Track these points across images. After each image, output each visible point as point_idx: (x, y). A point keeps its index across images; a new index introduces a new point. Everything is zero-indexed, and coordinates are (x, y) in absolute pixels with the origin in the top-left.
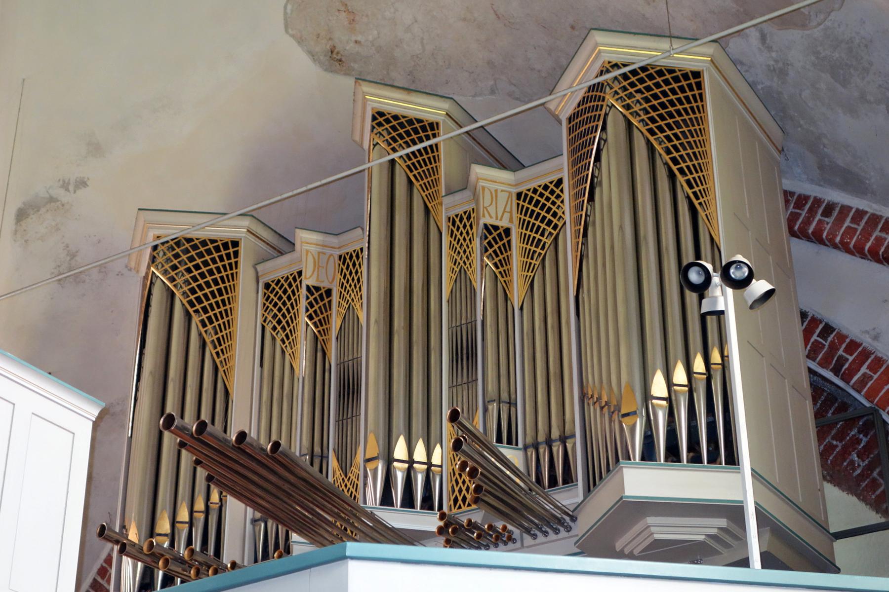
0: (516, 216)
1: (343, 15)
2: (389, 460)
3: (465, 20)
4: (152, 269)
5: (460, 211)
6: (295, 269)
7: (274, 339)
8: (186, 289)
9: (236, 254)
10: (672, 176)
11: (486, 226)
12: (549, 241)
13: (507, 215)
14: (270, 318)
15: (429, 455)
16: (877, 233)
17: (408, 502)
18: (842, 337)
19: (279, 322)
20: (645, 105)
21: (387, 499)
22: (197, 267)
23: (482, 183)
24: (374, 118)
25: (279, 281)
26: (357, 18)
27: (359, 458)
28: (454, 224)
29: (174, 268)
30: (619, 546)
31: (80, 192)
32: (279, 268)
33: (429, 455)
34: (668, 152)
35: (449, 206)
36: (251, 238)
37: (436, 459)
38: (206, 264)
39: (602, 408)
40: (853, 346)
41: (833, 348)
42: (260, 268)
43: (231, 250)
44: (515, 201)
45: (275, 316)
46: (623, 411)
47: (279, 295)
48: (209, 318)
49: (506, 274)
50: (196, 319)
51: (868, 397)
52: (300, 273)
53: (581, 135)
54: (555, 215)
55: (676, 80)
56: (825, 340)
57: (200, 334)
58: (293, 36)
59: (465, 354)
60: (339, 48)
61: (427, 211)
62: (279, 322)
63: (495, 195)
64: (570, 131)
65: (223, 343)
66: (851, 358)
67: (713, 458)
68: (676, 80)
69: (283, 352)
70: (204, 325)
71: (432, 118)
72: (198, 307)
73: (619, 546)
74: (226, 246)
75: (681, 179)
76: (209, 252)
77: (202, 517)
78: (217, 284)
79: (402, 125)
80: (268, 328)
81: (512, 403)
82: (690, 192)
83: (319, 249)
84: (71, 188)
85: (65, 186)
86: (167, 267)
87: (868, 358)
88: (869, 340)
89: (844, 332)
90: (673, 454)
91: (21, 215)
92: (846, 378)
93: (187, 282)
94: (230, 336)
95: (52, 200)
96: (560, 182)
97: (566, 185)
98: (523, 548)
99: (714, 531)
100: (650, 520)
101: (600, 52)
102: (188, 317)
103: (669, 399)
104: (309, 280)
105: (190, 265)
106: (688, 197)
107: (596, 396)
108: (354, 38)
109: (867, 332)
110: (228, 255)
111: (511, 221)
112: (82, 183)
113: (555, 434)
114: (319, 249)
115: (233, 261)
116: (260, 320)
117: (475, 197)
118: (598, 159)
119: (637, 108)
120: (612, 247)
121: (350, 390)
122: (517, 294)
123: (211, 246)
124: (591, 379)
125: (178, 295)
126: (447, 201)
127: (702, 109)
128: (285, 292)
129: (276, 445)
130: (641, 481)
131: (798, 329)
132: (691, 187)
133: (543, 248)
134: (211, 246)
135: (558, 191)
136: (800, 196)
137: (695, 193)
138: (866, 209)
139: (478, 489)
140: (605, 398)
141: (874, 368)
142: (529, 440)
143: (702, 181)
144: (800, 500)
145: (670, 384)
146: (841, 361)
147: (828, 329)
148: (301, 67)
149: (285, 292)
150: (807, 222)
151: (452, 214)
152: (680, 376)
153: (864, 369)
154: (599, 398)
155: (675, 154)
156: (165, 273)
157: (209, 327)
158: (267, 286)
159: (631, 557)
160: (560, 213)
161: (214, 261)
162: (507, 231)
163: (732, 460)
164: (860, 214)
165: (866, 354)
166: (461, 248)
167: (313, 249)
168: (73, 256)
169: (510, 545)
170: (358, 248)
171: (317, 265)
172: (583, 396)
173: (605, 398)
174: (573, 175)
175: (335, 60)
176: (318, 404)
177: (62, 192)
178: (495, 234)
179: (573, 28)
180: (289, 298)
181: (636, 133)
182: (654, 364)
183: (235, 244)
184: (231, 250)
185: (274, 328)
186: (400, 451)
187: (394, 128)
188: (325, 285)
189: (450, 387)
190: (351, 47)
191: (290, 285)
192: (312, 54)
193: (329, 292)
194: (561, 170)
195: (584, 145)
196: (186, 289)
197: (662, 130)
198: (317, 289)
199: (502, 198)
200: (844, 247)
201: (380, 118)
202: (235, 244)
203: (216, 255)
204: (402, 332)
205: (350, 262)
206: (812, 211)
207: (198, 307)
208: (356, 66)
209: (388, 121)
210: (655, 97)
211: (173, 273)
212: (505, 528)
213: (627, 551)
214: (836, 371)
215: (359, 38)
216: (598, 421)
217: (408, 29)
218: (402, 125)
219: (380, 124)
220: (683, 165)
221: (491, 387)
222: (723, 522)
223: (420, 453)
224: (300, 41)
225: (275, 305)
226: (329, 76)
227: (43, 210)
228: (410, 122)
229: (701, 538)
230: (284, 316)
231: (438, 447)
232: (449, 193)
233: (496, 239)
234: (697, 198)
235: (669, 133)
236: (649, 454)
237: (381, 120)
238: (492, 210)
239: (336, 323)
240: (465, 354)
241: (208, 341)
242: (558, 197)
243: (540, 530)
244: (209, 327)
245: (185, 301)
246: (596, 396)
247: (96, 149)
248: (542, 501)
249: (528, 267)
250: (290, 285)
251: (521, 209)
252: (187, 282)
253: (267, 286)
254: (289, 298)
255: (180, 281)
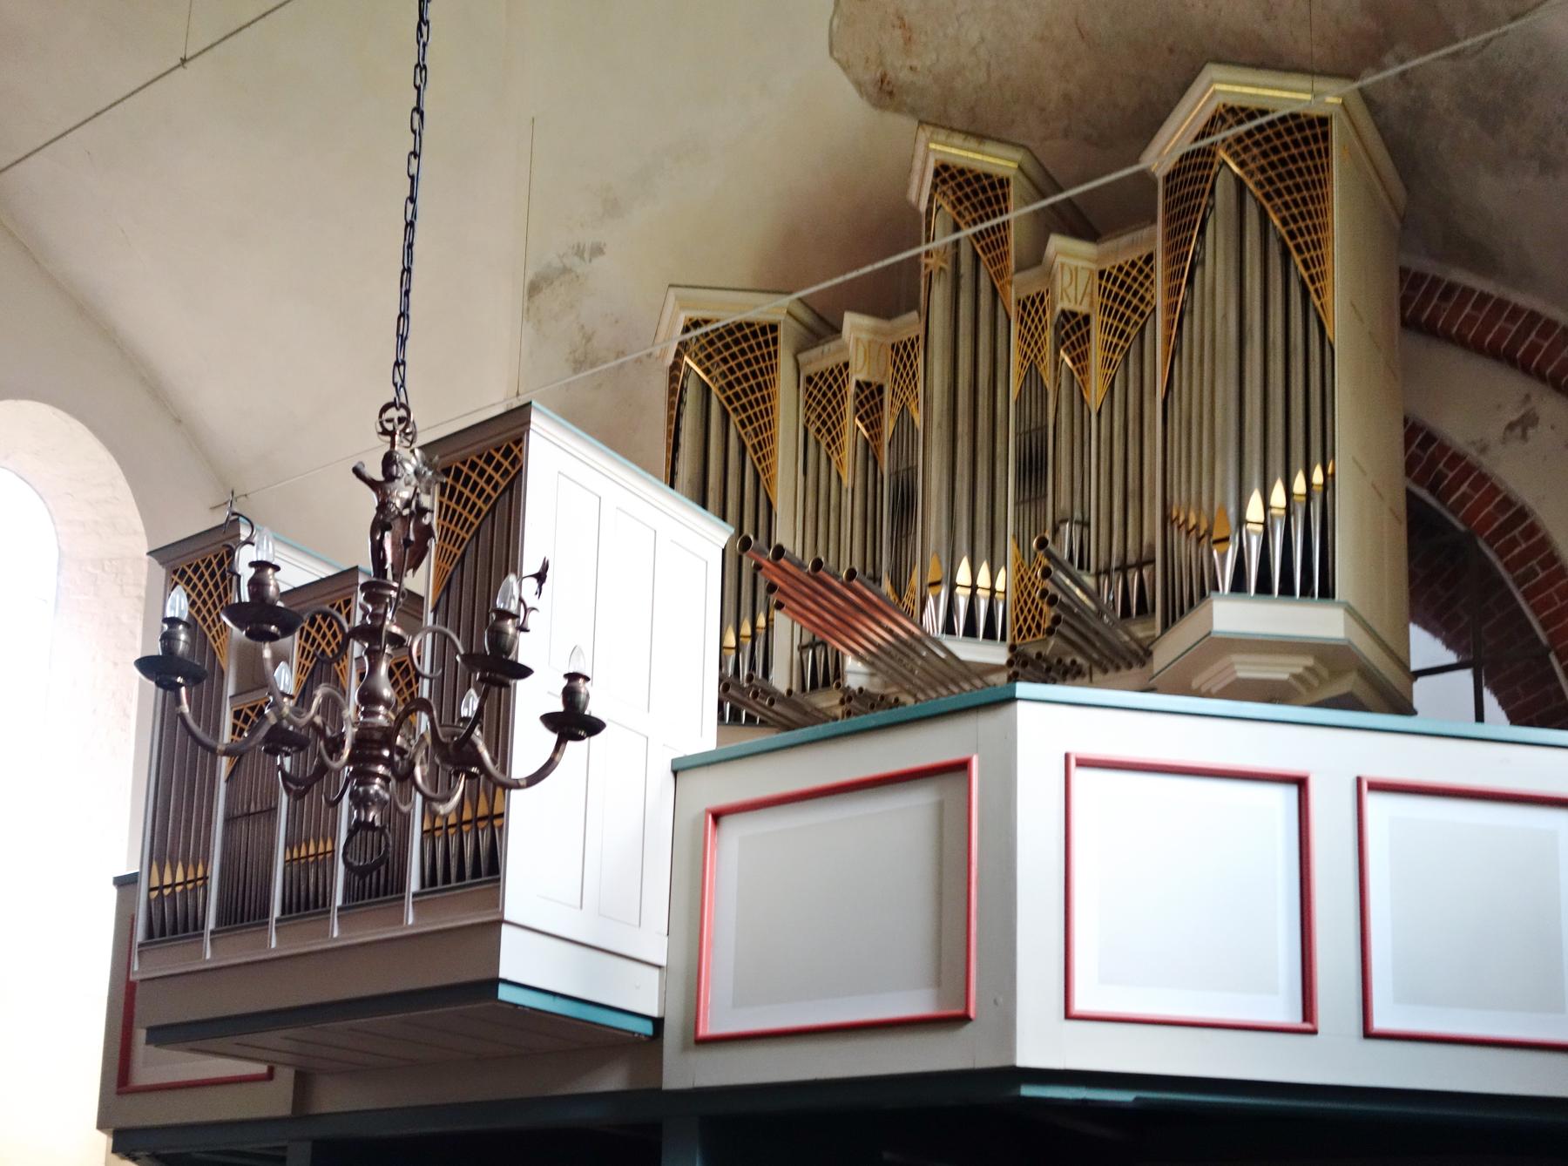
0: (1098, 299)
1: (898, 32)
2: (953, 586)
3: (1042, 39)
4: (686, 359)
5: (1033, 293)
6: (841, 360)
7: (818, 443)
8: (723, 382)
9: (775, 341)
10: (1286, 254)
11: (1063, 312)
12: (1134, 332)
13: (1086, 301)
14: (813, 418)
15: (993, 579)
16: (1500, 323)
17: (970, 631)
18: (1444, 448)
19: (824, 423)
20: (1263, 162)
21: (949, 629)
22: (734, 357)
23: (1059, 259)
24: (937, 173)
25: (822, 374)
26: (915, 36)
27: (916, 580)
28: (1024, 307)
29: (709, 357)
30: (1195, 685)
31: (597, 261)
32: (821, 359)
33: (993, 579)
34: (1284, 222)
35: (1017, 287)
36: (791, 321)
37: (1000, 586)
38: (743, 352)
39: (1188, 533)
40: (1456, 458)
41: (1433, 461)
42: (802, 357)
43: (770, 336)
44: (1097, 281)
45: (819, 416)
46: (1216, 536)
47: (823, 391)
48: (749, 418)
49: (1083, 371)
50: (734, 418)
51: (1463, 521)
52: (846, 365)
53: (1181, 200)
54: (1142, 299)
55: (1300, 128)
56: (1425, 450)
57: (739, 437)
58: (838, 61)
59: (1033, 468)
60: (891, 75)
61: (994, 292)
62: (824, 423)
63: (1075, 272)
64: (1167, 194)
65: (764, 447)
66: (1451, 475)
67: (1307, 591)
68: (1300, 128)
69: (829, 459)
70: (744, 426)
71: (1001, 173)
72: (737, 404)
73: (1195, 685)
74: (763, 330)
75: (1297, 259)
76: (746, 338)
77: (749, 642)
78: (755, 376)
79: (969, 183)
80: (812, 430)
81: (1085, 524)
82: (1306, 275)
83: (870, 337)
84: (586, 256)
85: (579, 252)
86: (701, 356)
87: (1470, 474)
88: (1474, 453)
89: (1448, 443)
90: (1264, 587)
91: (534, 289)
92: (1442, 499)
93: (724, 375)
94: (772, 439)
95: (565, 270)
96: (1149, 259)
97: (1159, 262)
98: (1092, 683)
99: (1299, 670)
100: (1235, 658)
101: (1215, 92)
102: (725, 416)
103: (1265, 524)
104: (858, 374)
105: (726, 354)
106: (1302, 282)
107: (1182, 519)
108: (908, 63)
109: (1473, 443)
110: (767, 342)
111: (1091, 304)
112: (598, 250)
113: (1132, 558)
114: (870, 337)
115: (772, 349)
116: (802, 421)
117: (1049, 275)
118: (1202, 231)
119: (1252, 166)
120: (1213, 340)
121: (905, 505)
122: (1095, 394)
123: (747, 331)
124: (1178, 496)
125: (714, 389)
126: (1017, 277)
127: (1326, 168)
128: (830, 387)
129: (818, 564)
130: (1230, 614)
131: (1399, 432)
132: (1307, 268)
133: (1127, 340)
134: (747, 331)
135: (1147, 270)
136: (1416, 274)
137: (1311, 277)
138: (1493, 292)
139: (1056, 620)
140: (1193, 521)
141: (1475, 486)
142: (1102, 565)
143: (1320, 260)
144: (1386, 637)
145: (1267, 506)
146: (1441, 476)
147: (1430, 438)
148: (844, 102)
149: (830, 387)
150: (1420, 308)
151: (1023, 296)
152: (1278, 497)
153: (1464, 488)
154: (1186, 521)
155: (1292, 226)
156: (699, 363)
157: (749, 428)
158: (809, 380)
159: (1208, 695)
160: (1148, 297)
161: (751, 349)
162: (1087, 319)
163: (1327, 592)
164: (1484, 298)
165: (1469, 469)
166: (1031, 339)
167: (865, 337)
168: (589, 340)
169: (1078, 680)
170: (913, 336)
171: (868, 356)
172: (1166, 518)
173: (1193, 521)
174: (1168, 251)
175: (885, 93)
176: (870, 520)
177: (576, 260)
178: (1073, 322)
179: (1171, 51)
180: (835, 395)
181: (1249, 201)
182: (1251, 484)
183: (774, 328)
184: (770, 336)
185: (819, 431)
186: (963, 576)
187: (960, 186)
188: (876, 379)
189: (1017, 504)
190: (904, 76)
191: (836, 380)
192: (859, 85)
193: (880, 389)
194: (1153, 239)
195: (1184, 214)
196: (723, 382)
197: (1280, 195)
198: (868, 385)
199: (1083, 277)
200: (1460, 341)
201: (945, 174)
202: (774, 328)
203: (753, 342)
204: (966, 438)
205: (903, 354)
206: (1460, 306)
207: (737, 404)
208: (909, 100)
209: (953, 177)
210: (1275, 150)
211: (708, 364)
212: (1074, 662)
213: (1204, 689)
214: (1432, 489)
215: (915, 63)
216: (1184, 548)
217: (973, 51)
218: (969, 183)
219: (944, 182)
220: (1300, 240)
221: (1064, 503)
222: (1310, 662)
223: (983, 579)
224: (846, 67)
225: (819, 403)
226: (875, 113)
227: (556, 283)
228: (978, 178)
229: (1285, 676)
230: (829, 416)
231: (1002, 572)
232: (1019, 269)
233: (1073, 328)
234: (1313, 282)
235: (1287, 198)
236: (1239, 585)
237: (946, 175)
238: (1071, 291)
239: (888, 426)
240: (1033, 468)
241: (748, 444)
242: (1147, 276)
243: (1112, 662)
244: (749, 428)
245: (722, 398)
246: (1182, 519)
247: (613, 208)
248: (1120, 632)
249: (1107, 363)
250: (836, 380)
251: (1104, 292)
252: (724, 375)
253: (809, 380)
254: (835, 395)
255: (716, 372)
